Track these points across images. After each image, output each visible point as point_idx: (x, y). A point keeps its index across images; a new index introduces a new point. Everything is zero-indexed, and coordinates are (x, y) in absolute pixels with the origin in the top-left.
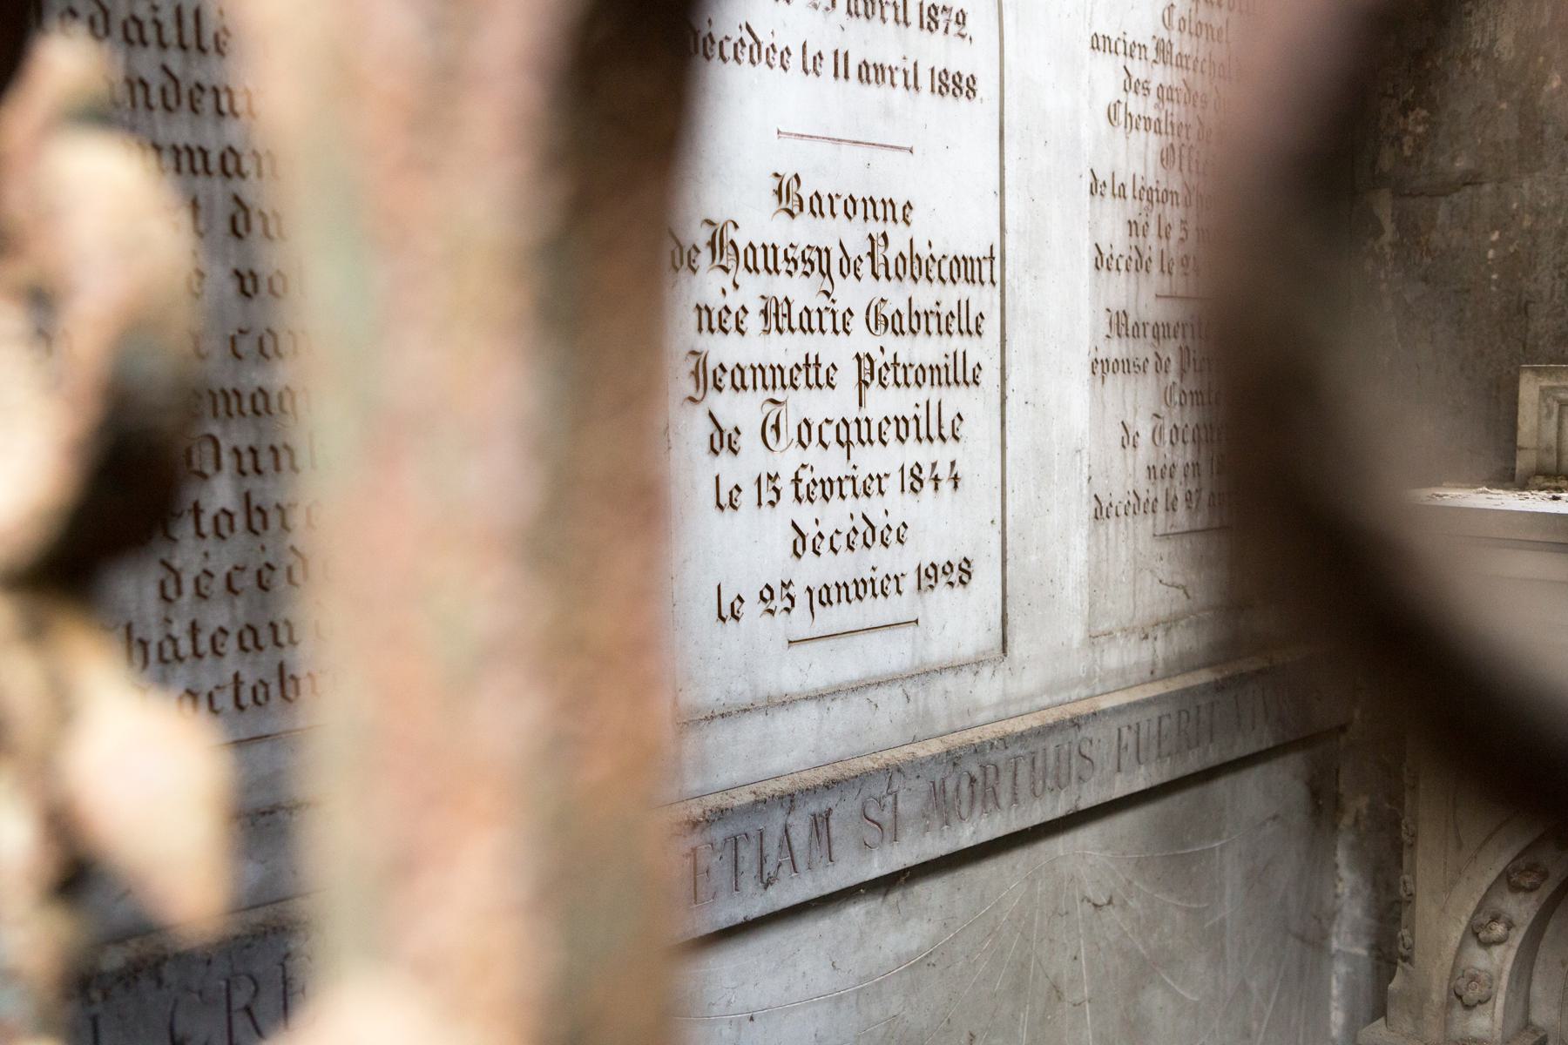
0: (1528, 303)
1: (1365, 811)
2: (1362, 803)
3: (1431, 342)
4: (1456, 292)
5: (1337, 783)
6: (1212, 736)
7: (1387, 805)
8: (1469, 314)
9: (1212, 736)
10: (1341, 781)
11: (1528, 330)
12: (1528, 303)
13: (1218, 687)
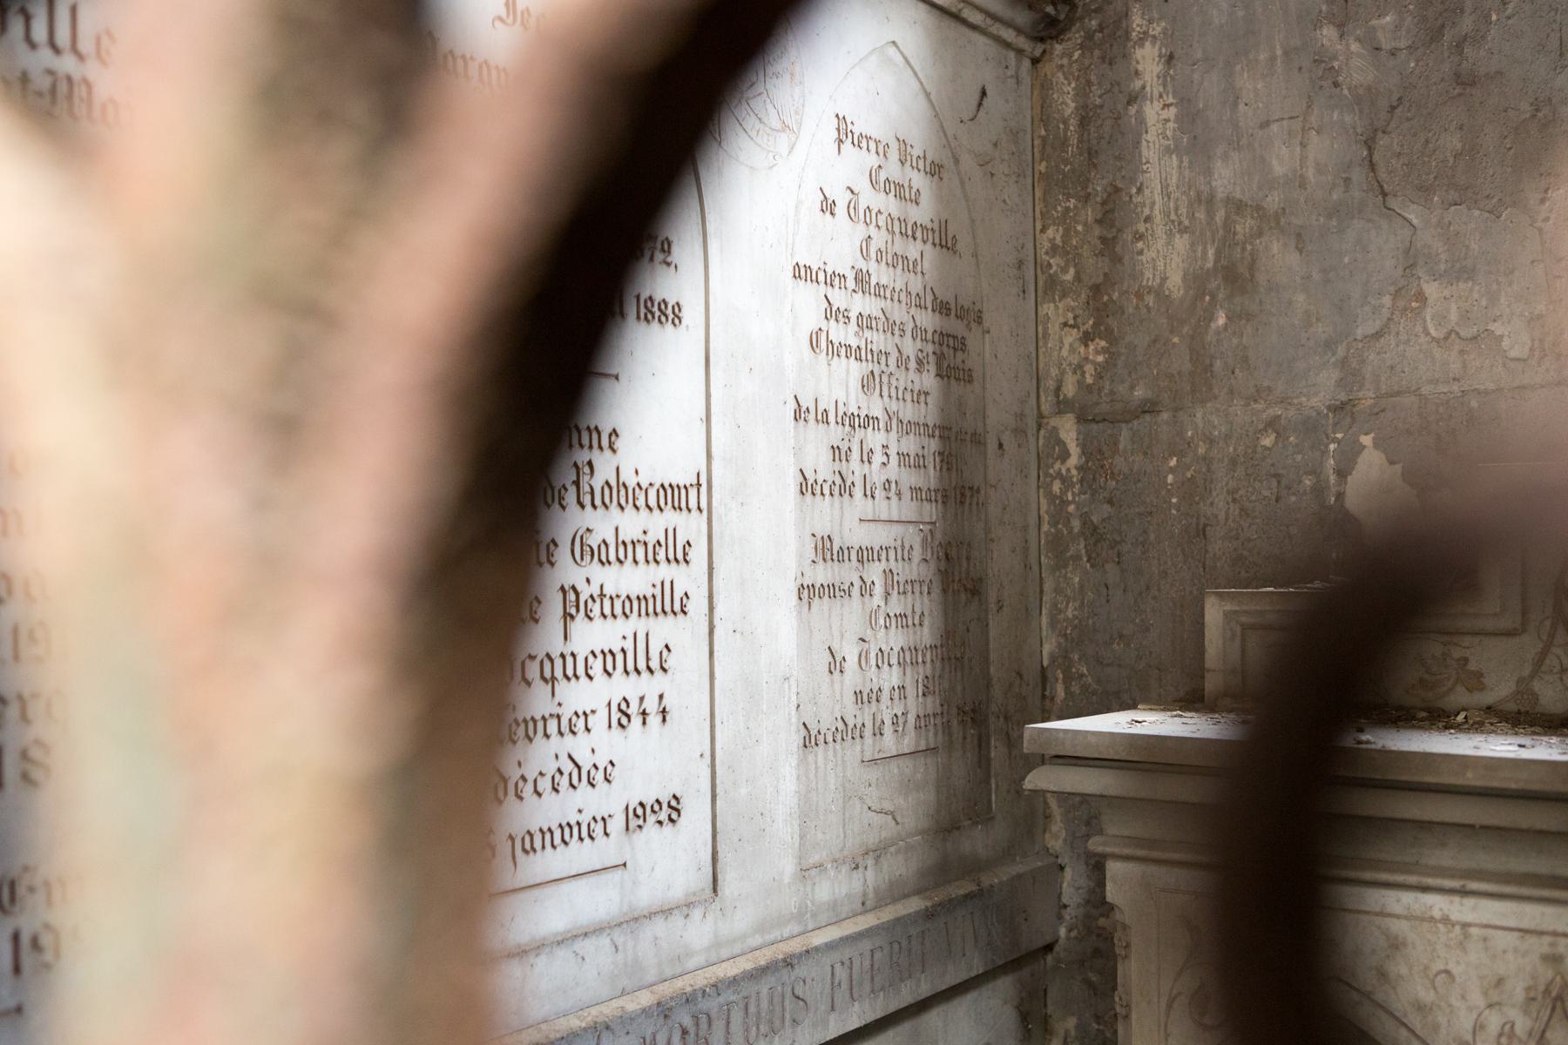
0: (1205, 525)
1: (1073, 1033)
2: (1071, 1022)
3: (1119, 562)
4: (1139, 514)
5: (1045, 1006)
6: (923, 966)
7: (1095, 1025)
8: (1152, 536)
9: (923, 966)
10: (1049, 1002)
11: (1206, 551)
12: (1205, 525)
13: (929, 915)
